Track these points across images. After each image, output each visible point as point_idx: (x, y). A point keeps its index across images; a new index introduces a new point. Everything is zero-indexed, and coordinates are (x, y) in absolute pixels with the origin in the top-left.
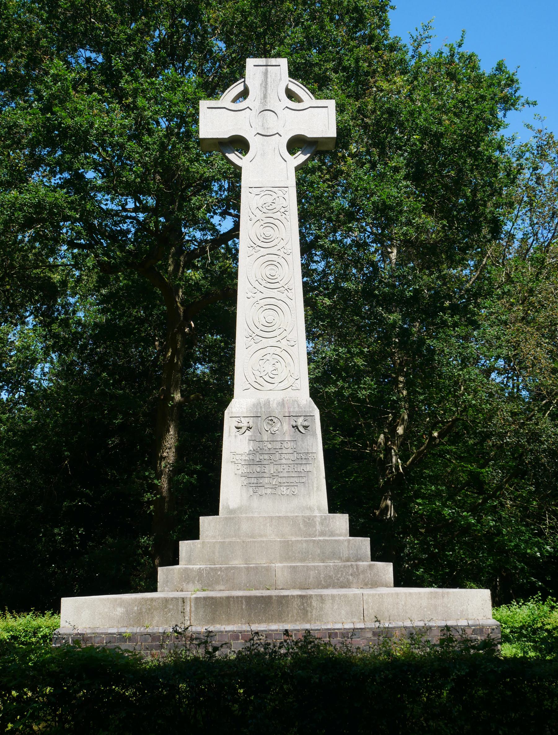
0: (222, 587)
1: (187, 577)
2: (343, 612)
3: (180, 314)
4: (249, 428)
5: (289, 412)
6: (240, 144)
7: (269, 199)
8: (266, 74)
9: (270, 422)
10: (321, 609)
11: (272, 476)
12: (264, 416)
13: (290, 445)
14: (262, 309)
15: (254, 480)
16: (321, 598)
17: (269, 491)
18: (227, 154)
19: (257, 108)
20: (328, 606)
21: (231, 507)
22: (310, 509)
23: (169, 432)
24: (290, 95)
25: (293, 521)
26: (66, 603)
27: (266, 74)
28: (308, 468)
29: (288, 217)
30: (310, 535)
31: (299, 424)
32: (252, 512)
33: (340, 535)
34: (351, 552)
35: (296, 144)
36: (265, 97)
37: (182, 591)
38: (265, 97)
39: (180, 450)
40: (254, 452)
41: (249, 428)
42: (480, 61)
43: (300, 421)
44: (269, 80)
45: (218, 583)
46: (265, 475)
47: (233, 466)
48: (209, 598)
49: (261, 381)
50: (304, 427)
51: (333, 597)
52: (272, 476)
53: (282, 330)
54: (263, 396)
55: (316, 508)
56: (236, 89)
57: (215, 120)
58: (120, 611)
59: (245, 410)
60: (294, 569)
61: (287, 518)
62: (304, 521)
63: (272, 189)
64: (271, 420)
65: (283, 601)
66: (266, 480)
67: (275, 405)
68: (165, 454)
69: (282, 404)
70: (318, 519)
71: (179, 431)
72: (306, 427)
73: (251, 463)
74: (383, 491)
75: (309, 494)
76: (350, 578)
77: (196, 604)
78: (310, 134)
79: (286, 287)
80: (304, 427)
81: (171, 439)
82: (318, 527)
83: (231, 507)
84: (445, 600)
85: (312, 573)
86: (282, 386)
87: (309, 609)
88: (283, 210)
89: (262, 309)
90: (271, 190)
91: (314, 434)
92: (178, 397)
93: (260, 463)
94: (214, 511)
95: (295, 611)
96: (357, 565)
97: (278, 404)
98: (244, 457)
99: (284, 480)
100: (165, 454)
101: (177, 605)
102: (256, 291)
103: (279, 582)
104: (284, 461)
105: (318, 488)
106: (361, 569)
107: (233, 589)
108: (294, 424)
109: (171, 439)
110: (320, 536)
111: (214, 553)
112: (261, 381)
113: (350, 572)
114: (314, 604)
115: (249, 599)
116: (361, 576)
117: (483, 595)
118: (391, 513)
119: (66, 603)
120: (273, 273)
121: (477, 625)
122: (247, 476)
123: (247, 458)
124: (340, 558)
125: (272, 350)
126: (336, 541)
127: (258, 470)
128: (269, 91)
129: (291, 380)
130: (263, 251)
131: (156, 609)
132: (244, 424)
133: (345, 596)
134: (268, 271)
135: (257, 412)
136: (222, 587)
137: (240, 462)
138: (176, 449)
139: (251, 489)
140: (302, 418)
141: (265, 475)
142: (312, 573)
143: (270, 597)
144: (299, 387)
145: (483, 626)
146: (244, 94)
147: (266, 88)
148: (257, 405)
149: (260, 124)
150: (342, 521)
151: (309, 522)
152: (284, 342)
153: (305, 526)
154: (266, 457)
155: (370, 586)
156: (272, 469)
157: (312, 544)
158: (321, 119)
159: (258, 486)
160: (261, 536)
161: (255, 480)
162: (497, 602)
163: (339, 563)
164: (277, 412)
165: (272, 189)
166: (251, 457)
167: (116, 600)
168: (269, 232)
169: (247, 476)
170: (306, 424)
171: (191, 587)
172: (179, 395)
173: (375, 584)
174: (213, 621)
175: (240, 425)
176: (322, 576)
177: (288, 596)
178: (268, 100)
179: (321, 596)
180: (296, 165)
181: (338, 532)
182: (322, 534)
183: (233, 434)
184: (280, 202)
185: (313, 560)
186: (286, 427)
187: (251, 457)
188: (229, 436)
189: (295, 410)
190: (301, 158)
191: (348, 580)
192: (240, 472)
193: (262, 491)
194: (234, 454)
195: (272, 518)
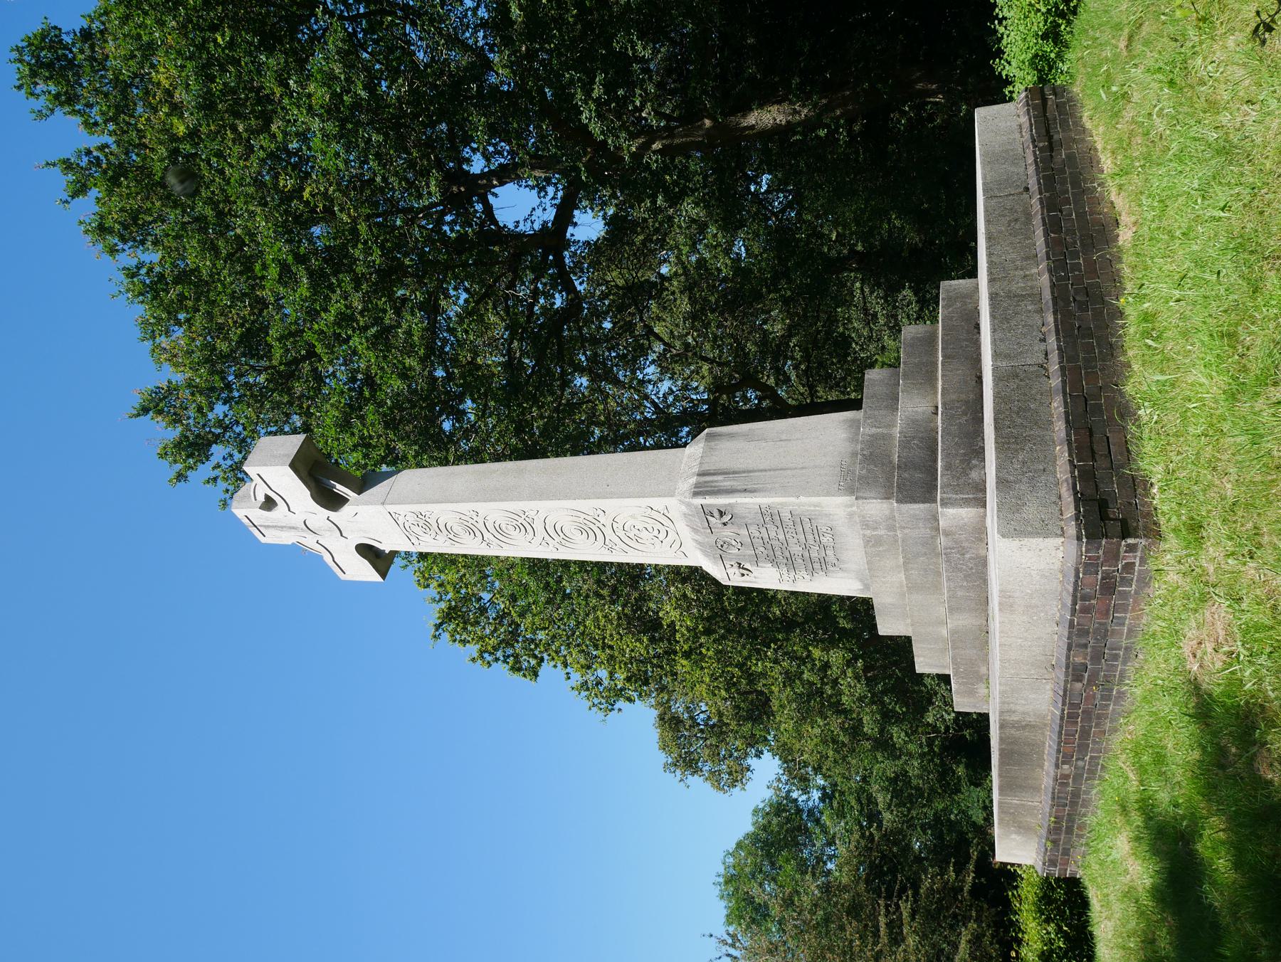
8: (267, 527)
15: (817, 566)
17: (830, 553)
62: (873, 546)
66: (814, 554)
70: (868, 532)
71: (746, 110)
72: (721, 514)
76: (967, 556)
85: (960, 593)
99: (810, 537)
104: (781, 537)
130: (486, 535)
161: (822, 565)
170: (716, 514)
184: (411, 518)
190: (340, 489)
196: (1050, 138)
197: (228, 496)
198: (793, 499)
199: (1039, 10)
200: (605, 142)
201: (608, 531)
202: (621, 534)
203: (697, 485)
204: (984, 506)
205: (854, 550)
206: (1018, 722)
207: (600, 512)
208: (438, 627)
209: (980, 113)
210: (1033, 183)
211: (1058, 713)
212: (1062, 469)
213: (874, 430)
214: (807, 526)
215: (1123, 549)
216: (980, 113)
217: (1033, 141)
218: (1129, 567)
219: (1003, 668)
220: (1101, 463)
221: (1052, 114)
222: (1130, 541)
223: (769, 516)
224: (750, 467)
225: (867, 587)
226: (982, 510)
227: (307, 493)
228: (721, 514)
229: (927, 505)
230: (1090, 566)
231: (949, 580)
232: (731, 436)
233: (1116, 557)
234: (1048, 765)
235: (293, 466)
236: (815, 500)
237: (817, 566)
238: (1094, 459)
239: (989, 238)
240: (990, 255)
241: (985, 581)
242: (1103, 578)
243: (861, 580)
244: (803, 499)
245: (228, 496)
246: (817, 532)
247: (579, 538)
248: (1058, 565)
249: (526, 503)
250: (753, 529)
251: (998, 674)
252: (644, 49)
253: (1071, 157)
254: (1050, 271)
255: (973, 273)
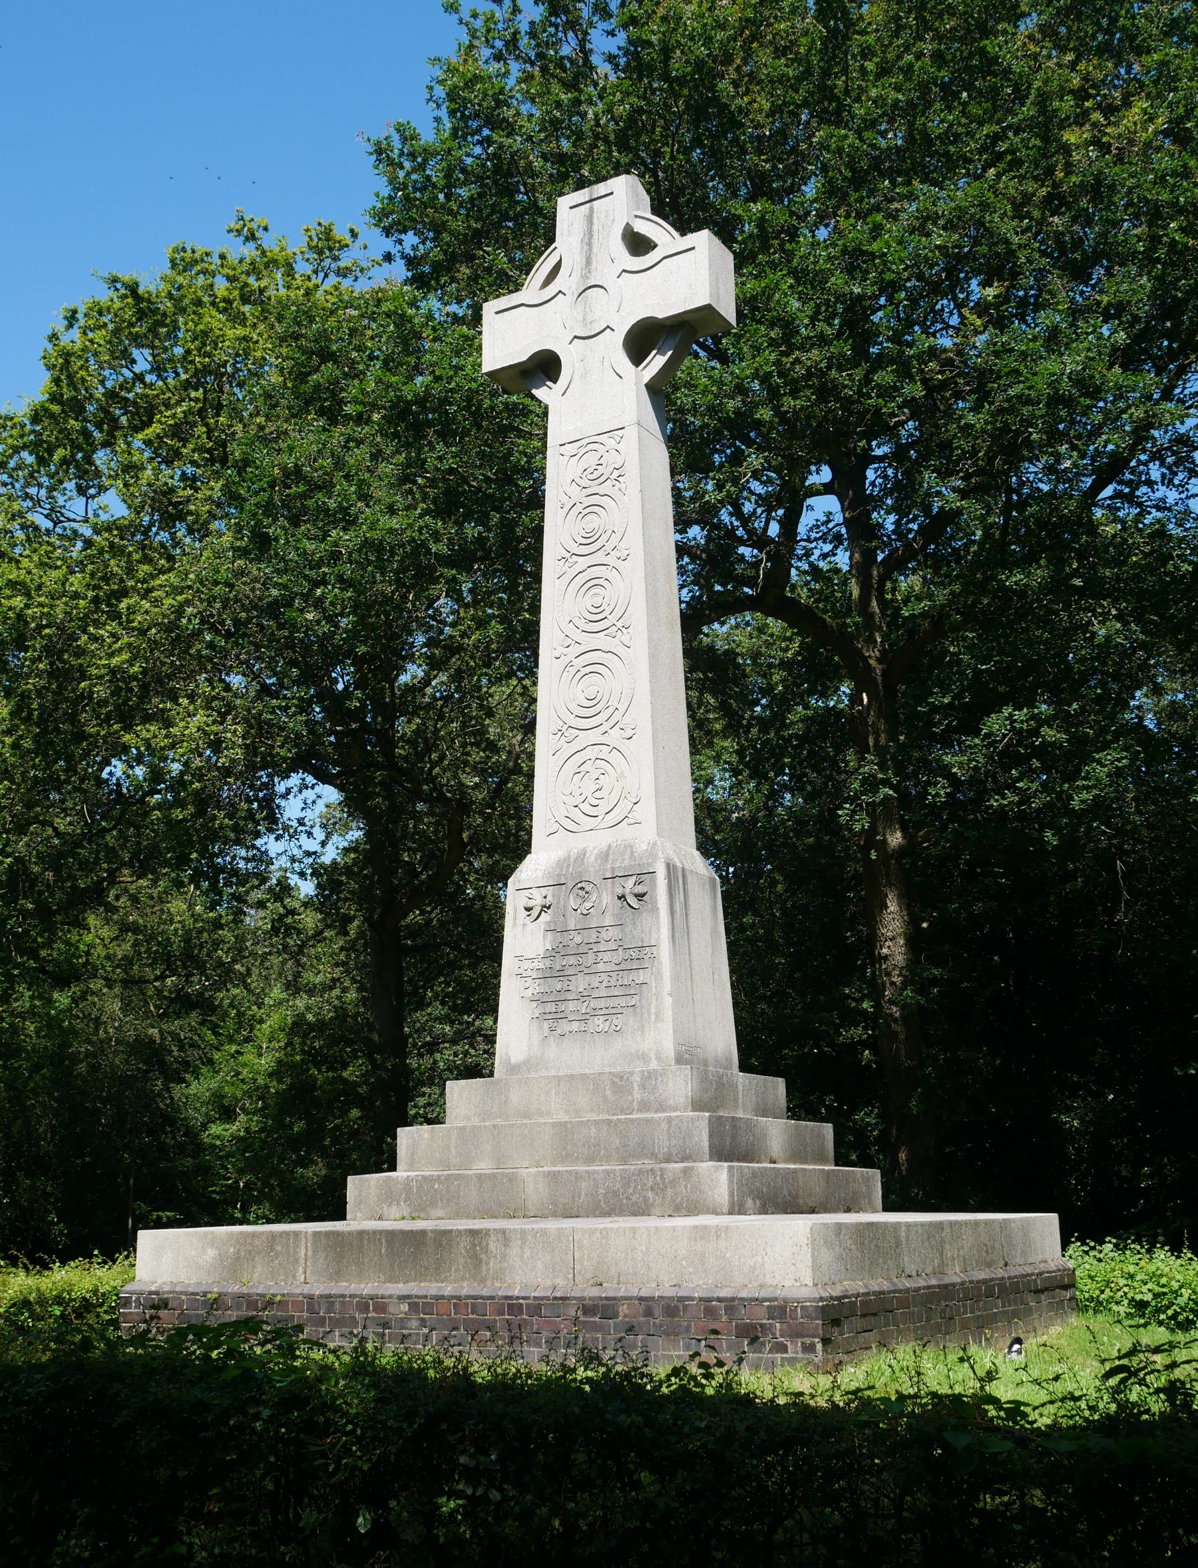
0: (440, 1213)
2: (539, 1265)
3: (875, 680)
4: (545, 908)
5: (613, 869)
7: (591, 460)
8: (590, 218)
9: (582, 893)
10: (504, 1256)
11: (582, 997)
13: (613, 933)
14: (579, 675)
15: (551, 1007)
17: (575, 1026)
18: (534, 391)
19: (574, 287)
20: (514, 1251)
21: (513, 1061)
22: (644, 1057)
23: (887, 907)
24: (638, 244)
25: (593, 1082)
26: (146, 1239)
28: (641, 977)
29: (623, 486)
30: (622, 1111)
31: (627, 891)
32: (547, 1069)
33: (675, 1109)
34: (674, 1142)
36: (588, 262)
37: (380, 1219)
38: (588, 262)
39: (914, 940)
41: (545, 908)
44: (595, 227)
45: (433, 1204)
46: (570, 996)
47: (520, 983)
48: (332, 1232)
49: (576, 814)
50: (636, 896)
51: (523, 1233)
52: (582, 997)
53: (611, 710)
54: (575, 844)
55: (653, 1056)
58: (211, 1253)
59: (540, 874)
60: (554, 1176)
61: (584, 1077)
62: (614, 1083)
63: (597, 439)
64: (581, 888)
66: (571, 1006)
67: (592, 859)
68: (885, 951)
69: (605, 856)
70: (637, 1078)
71: (909, 902)
72: (640, 896)
73: (547, 975)
74: (903, 1007)
75: (642, 1029)
76: (650, 1194)
77: (314, 1243)
78: (663, 311)
79: (619, 624)
80: (636, 896)
81: (893, 919)
82: (637, 1094)
83: (513, 1061)
84: (722, 1243)
85: (584, 1185)
86: (612, 819)
87: (483, 1257)
88: (616, 473)
89: (579, 675)
91: (655, 910)
93: (561, 974)
94: (476, 1071)
95: (462, 1261)
96: (661, 1170)
97: (599, 855)
98: (536, 965)
99: (602, 1003)
100: (885, 951)
101: (288, 1245)
102: (569, 641)
103: (529, 1205)
104: (601, 967)
105: (657, 1015)
106: (669, 1176)
107: (457, 1215)
108: (620, 892)
109: (893, 919)
110: (640, 1111)
111: (448, 1148)
112: (576, 814)
113: (650, 1184)
114: (492, 1247)
116: (669, 1192)
119: (146, 1239)
120: (598, 601)
121: (776, 1299)
122: (539, 1000)
123: (541, 966)
124: (654, 1155)
125: (591, 753)
126: (647, 1120)
127: (559, 987)
128: (595, 250)
129: (624, 807)
130: (583, 563)
131: (259, 1252)
132: (538, 902)
133: (544, 1232)
134: (588, 601)
135: (559, 875)
136: (440, 1213)
137: (529, 973)
138: (906, 940)
139: (546, 1025)
140: (632, 880)
141: (570, 996)
142: (584, 1185)
143: (423, 1233)
144: (639, 819)
145: (785, 1301)
147: (590, 244)
148: (563, 863)
149: (580, 318)
152: (615, 732)
153: (615, 1092)
154: (572, 960)
155: (684, 1212)
156: (580, 984)
157: (605, 1128)
158: (694, 273)
159: (559, 1016)
160: (541, 1114)
161: (552, 1010)
165: (597, 439)
166: (548, 963)
167: (206, 1234)
168: (592, 522)
169: (539, 1000)
170: (640, 889)
171: (394, 1212)
172: (899, 834)
174: (337, 1275)
175: (530, 904)
176: (601, 1191)
177: (451, 1231)
178: (593, 267)
179: (503, 1232)
180: (646, 380)
181: (671, 1102)
182: (644, 1106)
183: (520, 922)
184: (612, 459)
185: (608, 1159)
186: (607, 899)
187: (548, 963)
188: (515, 925)
190: (656, 362)
191: (646, 1199)
192: (529, 993)
193: (564, 1027)
194: (520, 958)
195: (559, 1079)
196: (1042, 1291)
197: (466, 16)
198: (667, 987)
199: (1102, 1292)
200: (976, 732)
201: (594, 736)
202: (591, 753)
203: (675, 866)
204: (730, 1213)
205: (592, 1056)
206: (486, 1250)
207: (629, 733)
208: (133, 289)
209: (1053, 1219)
210: (1014, 1271)
211: (516, 1293)
212: (856, 1286)
213: (740, 1088)
214: (622, 1002)
215: (808, 1341)
216: (1053, 1219)
217: (1041, 1274)
218: (783, 1348)
219: (592, 1232)
220: (858, 1323)
221: (1057, 1290)
222: (819, 1347)
223: (637, 957)
224: (692, 935)
225: (514, 1069)
226: (725, 1209)
227: (661, 314)
228: (640, 896)
229: (707, 1150)
230: (780, 1309)
231: (608, 1172)
232: (715, 911)
233: (795, 1334)
234: (399, 1288)
235: (708, 308)
236: (668, 1014)
237: (551, 1007)
238: (863, 1316)
239: (977, 1223)
240: (966, 1223)
241: (607, 1214)
242: (762, 1326)
243: (526, 1062)
244: (668, 1001)
245: (466, 16)
246: (611, 1013)
247: (580, 692)
248: (769, 1280)
249: (645, 635)
250: (613, 933)
251: (609, 1226)
252: (1082, 801)
253: (1029, 1311)
254: (963, 1283)
255: (886, 1209)
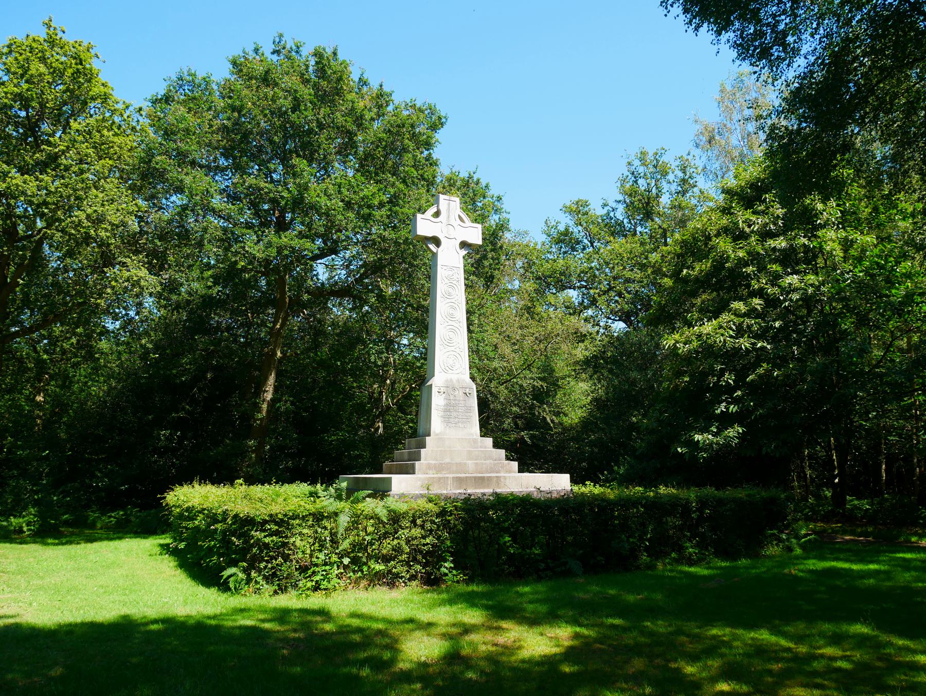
1: (429, 467)
6: (437, 241)
7: (451, 273)
8: (449, 204)
12: (450, 388)
16: (505, 478)
20: (507, 481)
27: (449, 204)
35: (464, 245)
40: (447, 405)
42: (499, 199)
43: (467, 391)
54: (449, 376)
56: (433, 210)
57: (425, 226)
65: (489, 478)
69: (458, 381)
71: (277, 376)
73: (445, 411)
78: (470, 241)
81: (272, 380)
90: (452, 268)
92: (279, 354)
93: (449, 411)
109: (272, 380)
115: (475, 478)
117: (566, 477)
118: (381, 431)
132: (442, 391)
146: (437, 214)
148: (447, 381)
150: (489, 441)
151: (475, 441)
161: (447, 419)
162: (574, 481)
163: (492, 462)
164: (457, 385)
168: (451, 290)
171: (431, 472)
173: (510, 472)
186: (461, 393)
189: (465, 385)
